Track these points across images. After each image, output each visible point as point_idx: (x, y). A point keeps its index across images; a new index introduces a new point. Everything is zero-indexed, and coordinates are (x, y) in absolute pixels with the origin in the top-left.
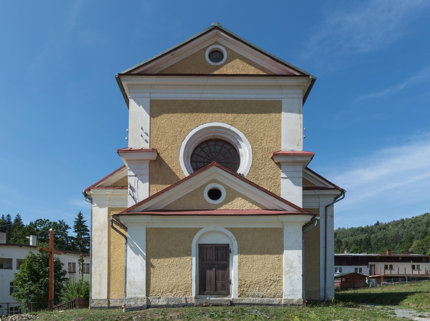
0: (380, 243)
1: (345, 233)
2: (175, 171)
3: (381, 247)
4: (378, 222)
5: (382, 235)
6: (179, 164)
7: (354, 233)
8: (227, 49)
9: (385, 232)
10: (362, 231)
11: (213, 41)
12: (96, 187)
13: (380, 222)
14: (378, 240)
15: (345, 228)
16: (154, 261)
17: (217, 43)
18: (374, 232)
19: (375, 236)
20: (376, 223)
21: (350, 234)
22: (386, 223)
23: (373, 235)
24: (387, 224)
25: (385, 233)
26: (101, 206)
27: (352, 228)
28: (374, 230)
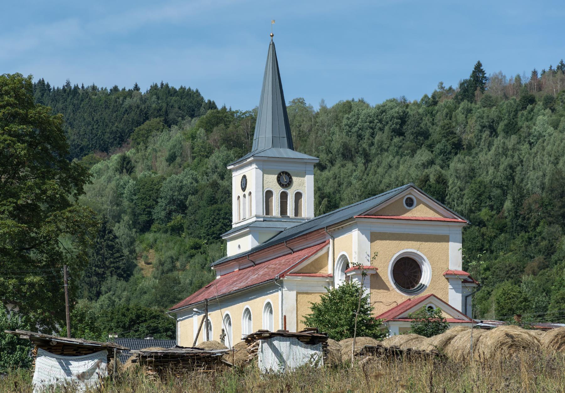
0: (492, 208)
1: (312, 136)
2: (385, 282)
3: (496, 237)
4: (478, 68)
5: (502, 167)
6: (387, 277)
7: (360, 137)
8: (416, 198)
9: (514, 149)
10: (400, 133)
11: (408, 192)
12: (288, 274)
13: (489, 71)
14: (480, 195)
15: (308, 103)
16: (219, 341)
17: (410, 194)
18: (460, 141)
19: (467, 168)
20: (467, 75)
21: (336, 146)
22: (518, 79)
23: (460, 166)
24: (524, 82)
25: (513, 157)
26: (290, 290)
27: (348, 107)
28: (458, 130)
